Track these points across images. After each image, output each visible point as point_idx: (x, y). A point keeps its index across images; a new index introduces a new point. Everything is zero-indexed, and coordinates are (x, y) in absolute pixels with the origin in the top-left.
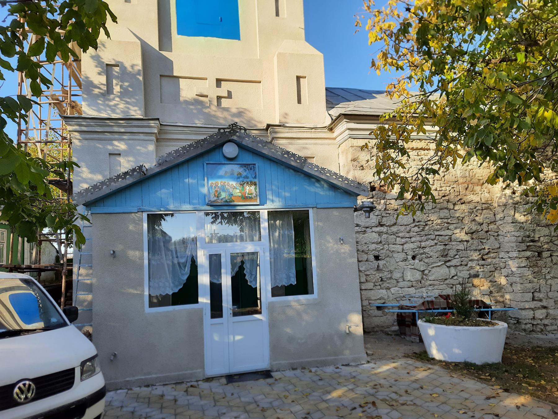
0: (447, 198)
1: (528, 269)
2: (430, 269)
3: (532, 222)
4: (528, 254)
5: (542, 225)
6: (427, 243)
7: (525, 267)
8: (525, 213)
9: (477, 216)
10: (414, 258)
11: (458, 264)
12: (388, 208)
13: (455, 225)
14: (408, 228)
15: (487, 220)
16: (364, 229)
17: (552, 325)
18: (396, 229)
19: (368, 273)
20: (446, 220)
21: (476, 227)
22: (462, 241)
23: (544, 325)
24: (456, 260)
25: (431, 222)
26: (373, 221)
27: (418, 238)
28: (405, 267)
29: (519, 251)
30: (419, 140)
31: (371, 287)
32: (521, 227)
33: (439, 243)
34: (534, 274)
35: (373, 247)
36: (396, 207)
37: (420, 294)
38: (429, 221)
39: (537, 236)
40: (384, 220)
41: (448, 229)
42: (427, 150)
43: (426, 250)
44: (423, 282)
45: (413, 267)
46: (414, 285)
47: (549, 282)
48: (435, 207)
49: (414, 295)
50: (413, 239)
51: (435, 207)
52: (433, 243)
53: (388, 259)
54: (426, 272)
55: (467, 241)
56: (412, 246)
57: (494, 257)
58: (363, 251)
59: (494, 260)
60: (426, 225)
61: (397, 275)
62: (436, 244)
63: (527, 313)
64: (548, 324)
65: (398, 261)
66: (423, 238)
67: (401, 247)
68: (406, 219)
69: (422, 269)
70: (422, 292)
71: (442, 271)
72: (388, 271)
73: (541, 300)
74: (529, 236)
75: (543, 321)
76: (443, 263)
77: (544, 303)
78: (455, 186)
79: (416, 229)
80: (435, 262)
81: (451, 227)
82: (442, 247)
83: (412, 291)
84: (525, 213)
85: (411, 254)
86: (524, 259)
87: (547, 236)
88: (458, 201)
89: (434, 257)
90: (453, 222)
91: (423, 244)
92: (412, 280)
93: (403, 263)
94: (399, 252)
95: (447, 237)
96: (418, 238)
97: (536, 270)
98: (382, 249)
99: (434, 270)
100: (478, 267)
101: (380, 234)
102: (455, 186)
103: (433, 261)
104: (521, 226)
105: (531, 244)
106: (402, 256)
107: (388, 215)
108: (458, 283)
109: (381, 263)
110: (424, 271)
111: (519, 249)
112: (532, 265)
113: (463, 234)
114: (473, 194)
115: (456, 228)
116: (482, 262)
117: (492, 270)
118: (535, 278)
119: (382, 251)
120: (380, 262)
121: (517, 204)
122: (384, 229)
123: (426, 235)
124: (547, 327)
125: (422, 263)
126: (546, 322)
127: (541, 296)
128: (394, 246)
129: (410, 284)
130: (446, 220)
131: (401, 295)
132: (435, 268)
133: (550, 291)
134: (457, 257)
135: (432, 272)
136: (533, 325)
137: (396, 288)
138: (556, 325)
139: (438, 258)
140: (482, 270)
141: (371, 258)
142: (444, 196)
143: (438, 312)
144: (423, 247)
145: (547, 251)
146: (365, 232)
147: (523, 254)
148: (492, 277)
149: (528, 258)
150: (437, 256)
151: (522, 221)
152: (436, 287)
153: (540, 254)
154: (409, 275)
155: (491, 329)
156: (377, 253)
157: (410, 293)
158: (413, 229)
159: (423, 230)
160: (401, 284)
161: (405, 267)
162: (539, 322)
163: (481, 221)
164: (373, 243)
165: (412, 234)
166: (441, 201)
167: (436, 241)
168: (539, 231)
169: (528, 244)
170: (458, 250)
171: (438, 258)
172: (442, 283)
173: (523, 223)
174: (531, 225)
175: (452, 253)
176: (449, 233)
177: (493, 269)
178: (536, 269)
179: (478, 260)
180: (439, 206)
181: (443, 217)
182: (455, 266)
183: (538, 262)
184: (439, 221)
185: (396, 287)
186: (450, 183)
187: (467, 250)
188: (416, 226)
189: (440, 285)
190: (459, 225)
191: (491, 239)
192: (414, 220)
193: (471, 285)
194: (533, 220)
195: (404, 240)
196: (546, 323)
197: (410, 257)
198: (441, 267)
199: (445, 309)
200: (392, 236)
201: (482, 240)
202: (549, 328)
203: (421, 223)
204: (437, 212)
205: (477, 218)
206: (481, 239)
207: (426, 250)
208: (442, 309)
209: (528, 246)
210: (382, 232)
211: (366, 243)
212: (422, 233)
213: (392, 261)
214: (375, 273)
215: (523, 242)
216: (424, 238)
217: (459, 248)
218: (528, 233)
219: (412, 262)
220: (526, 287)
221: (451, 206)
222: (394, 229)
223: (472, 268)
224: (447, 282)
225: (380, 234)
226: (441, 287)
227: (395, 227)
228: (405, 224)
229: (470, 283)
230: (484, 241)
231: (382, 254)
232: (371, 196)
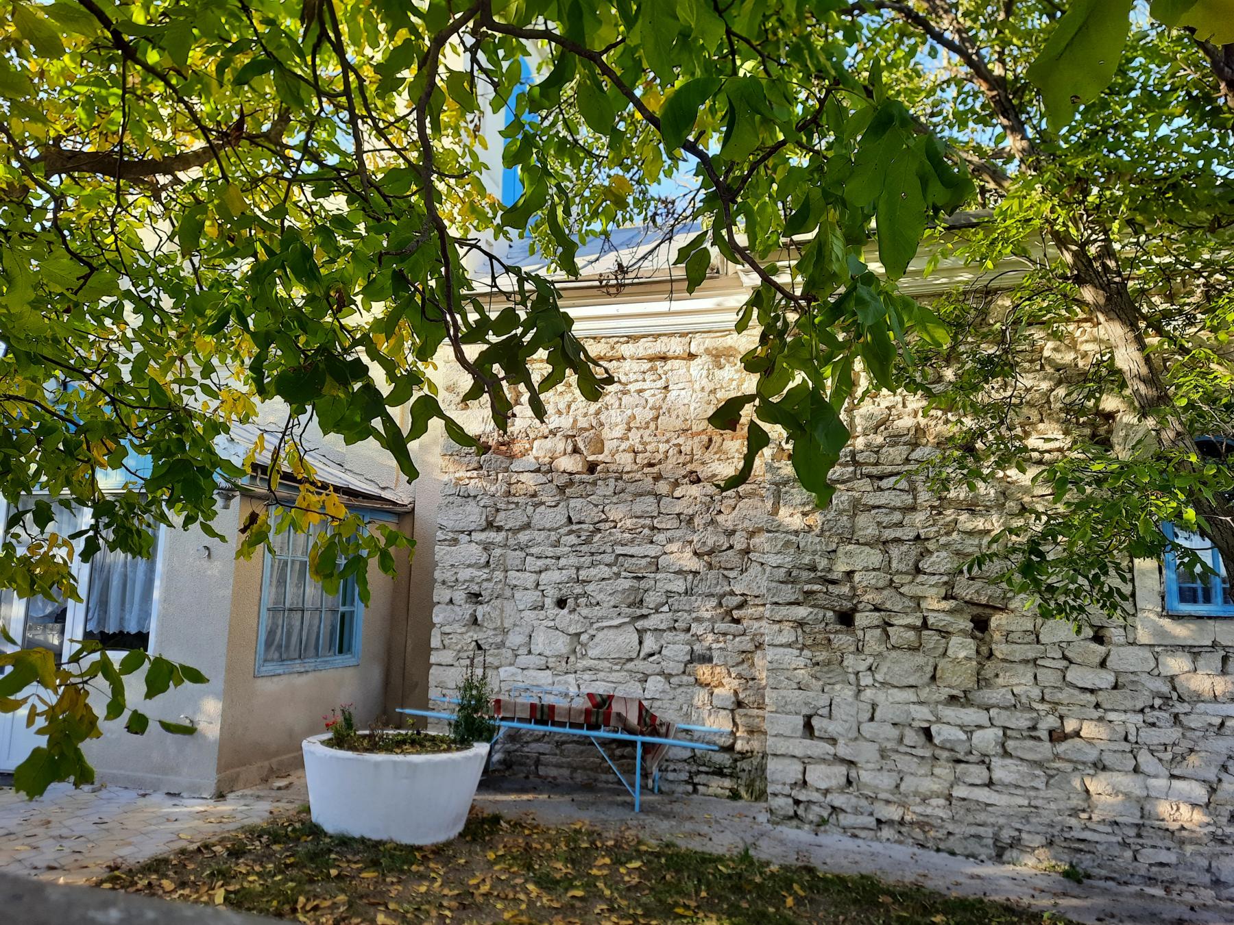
0: (655, 470)
1: (797, 652)
2: (593, 633)
3: (822, 531)
4: (802, 612)
5: (861, 541)
6: (593, 572)
7: (789, 646)
8: (807, 508)
9: (720, 512)
10: (561, 603)
11: (663, 626)
12: (513, 491)
13: (669, 534)
14: (554, 536)
15: (746, 524)
16: (451, 535)
17: (857, 811)
18: (527, 538)
19: (447, 629)
20: (648, 521)
21: (715, 538)
22: (680, 572)
23: (833, 808)
24: (661, 616)
25: (608, 525)
26: (472, 518)
27: (573, 560)
28: (536, 623)
29: (776, 603)
30: (594, 338)
31: (450, 661)
32: (787, 544)
33: (624, 574)
34: (817, 668)
35: (465, 574)
36: (531, 490)
37: (562, 688)
38: (606, 521)
39: (841, 567)
40: (500, 519)
41: (652, 542)
42: (618, 360)
43: (590, 588)
44: (572, 659)
45: (552, 624)
46: (550, 665)
47: (868, 694)
48: (623, 491)
49: (550, 688)
50: (563, 562)
51: (623, 491)
52: (606, 571)
53: (497, 602)
54: (584, 638)
55: (696, 573)
56: (555, 576)
57: (756, 615)
58: (444, 583)
59: (756, 625)
60: (599, 530)
61: (515, 639)
62: (618, 575)
63: (780, 767)
64: (844, 807)
65: (521, 607)
66: (583, 559)
67: (534, 576)
68: (551, 517)
69: (572, 630)
70: (566, 682)
71: (620, 639)
72: (495, 629)
73: (833, 741)
74: (813, 569)
75: (829, 797)
76: (627, 620)
77: (843, 750)
78: (681, 441)
79: (572, 539)
80: (606, 618)
81: (660, 538)
82: (627, 584)
83: (545, 678)
84: (807, 508)
85: (552, 594)
86: (787, 627)
87: (874, 569)
88: (684, 477)
89: (605, 605)
90: (663, 526)
91: (583, 574)
92: (547, 653)
93: (533, 614)
94: (526, 589)
95: (644, 562)
96: (573, 560)
97: (821, 658)
98: (487, 580)
99: (600, 635)
100: (710, 637)
101: (487, 547)
102: (681, 441)
103: (600, 614)
104: (792, 541)
105: (816, 587)
106: (533, 596)
107: (513, 506)
108: (658, 670)
109: (481, 611)
110: (578, 635)
111: (775, 599)
112: (809, 642)
113: (688, 553)
114: (719, 460)
115: (670, 541)
116: (721, 626)
117: (744, 648)
118: (817, 679)
119: (485, 585)
120: (480, 608)
121: (785, 483)
122: (499, 537)
123: (592, 554)
124: (841, 816)
125: (575, 617)
126: (838, 800)
127: (833, 728)
128: (518, 574)
129: (542, 662)
130: (648, 521)
131: (520, 684)
132: (605, 631)
133: (872, 719)
134: (666, 608)
135: (596, 640)
136: (797, 802)
137: (512, 669)
138: (871, 814)
139: (615, 607)
140: (721, 645)
141: (460, 596)
142: (651, 465)
143: (581, 736)
144: (584, 581)
145: (871, 611)
146: (455, 542)
147: (784, 612)
148: (745, 666)
149: (801, 624)
150: (612, 603)
151: (795, 528)
152: (601, 675)
153: (846, 619)
154: (541, 642)
155: (350, 759)
156: (475, 588)
157: (540, 683)
158: (564, 539)
159: (588, 542)
160: (523, 660)
161: (536, 623)
162: (816, 796)
163: (730, 525)
164: (469, 566)
165: (559, 551)
166: (638, 476)
167: (615, 569)
168: (849, 554)
169: (806, 588)
170: (669, 594)
171: (615, 607)
172: (618, 667)
173: (796, 533)
174: (818, 539)
175: (652, 599)
176: (652, 551)
177: (750, 647)
178: (822, 656)
179: (712, 620)
180: (631, 488)
181: (639, 514)
182: (656, 630)
183: (832, 636)
184: (629, 523)
185: (511, 665)
186: (668, 434)
187: (692, 595)
188: (571, 532)
189: (611, 671)
190: (678, 533)
191: (750, 570)
192: (569, 518)
193: (692, 679)
194: (826, 527)
195: (540, 563)
196: (836, 803)
197: (549, 602)
198: (620, 631)
199: (580, 726)
200: (518, 552)
201: (726, 573)
202: (846, 820)
203: (583, 526)
204: (626, 501)
205: (720, 518)
206: (726, 569)
207: (590, 588)
208: (572, 725)
209: (809, 593)
210: (492, 543)
211: (452, 566)
212: (584, 548)
213: (509, 607)
214: (464, 630)
215: (790, 579)
216: (587, 560)
217: (670, 587)
218: (807, 560)
219: (553, 611)
220: (783, 697)
221: (663, 487)
222: (523, 537)
223: (698, 638)
224: (630, 666)
225: (487, 547)
226: (615, 676)
227: (527, 532)
228: (547, 526)
229: (690, 675)
230: (731, 574)
231: (487, 589)
232: (474, 465)
